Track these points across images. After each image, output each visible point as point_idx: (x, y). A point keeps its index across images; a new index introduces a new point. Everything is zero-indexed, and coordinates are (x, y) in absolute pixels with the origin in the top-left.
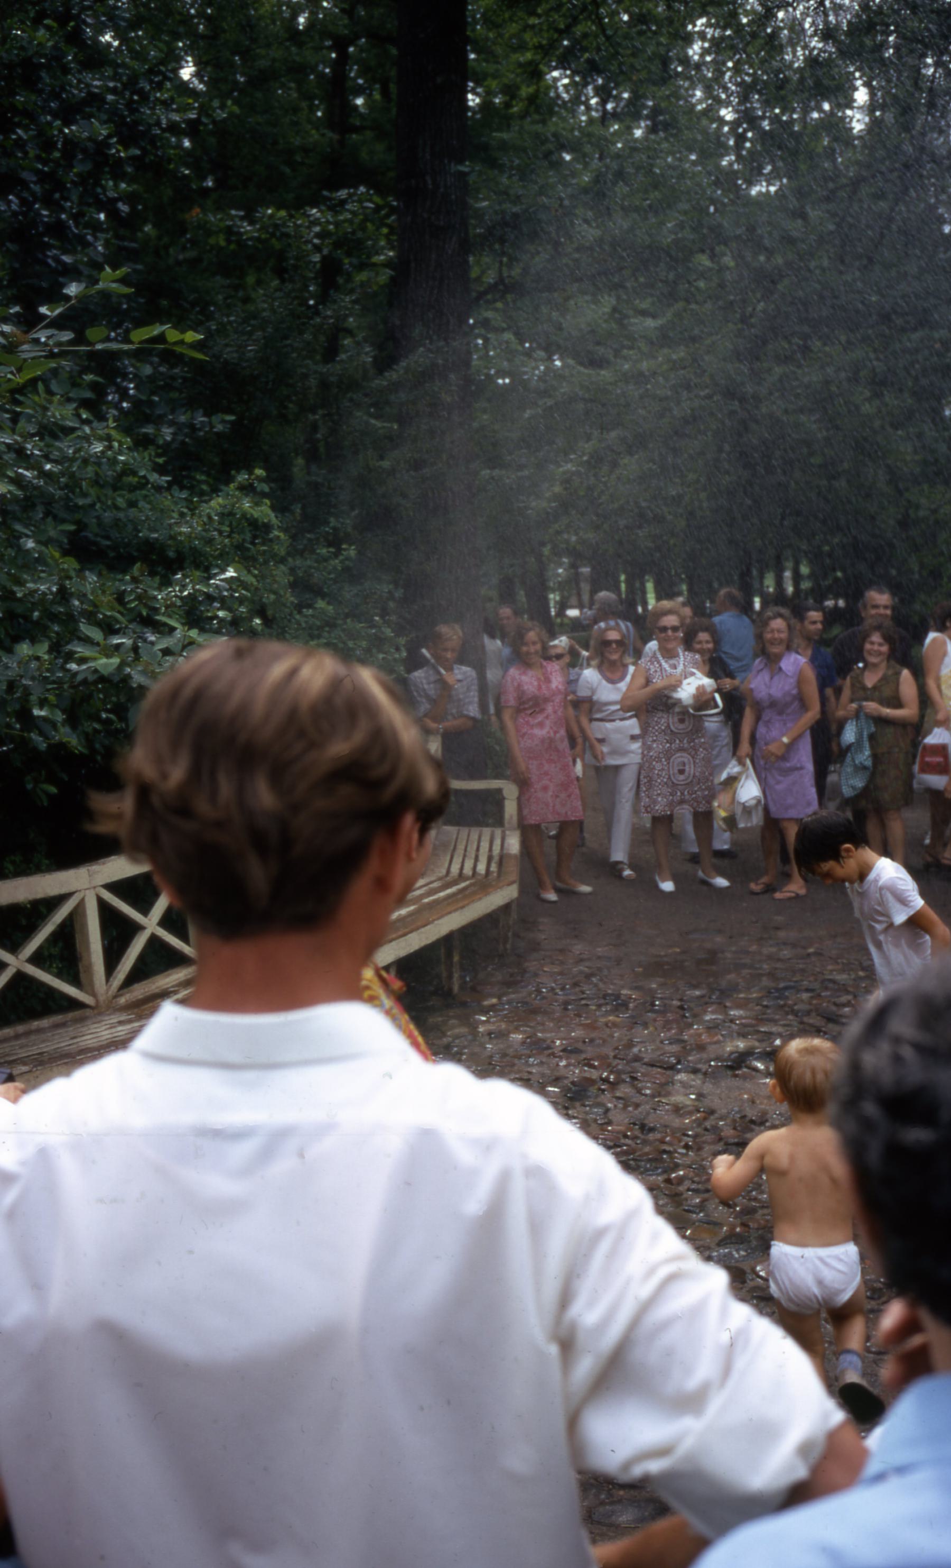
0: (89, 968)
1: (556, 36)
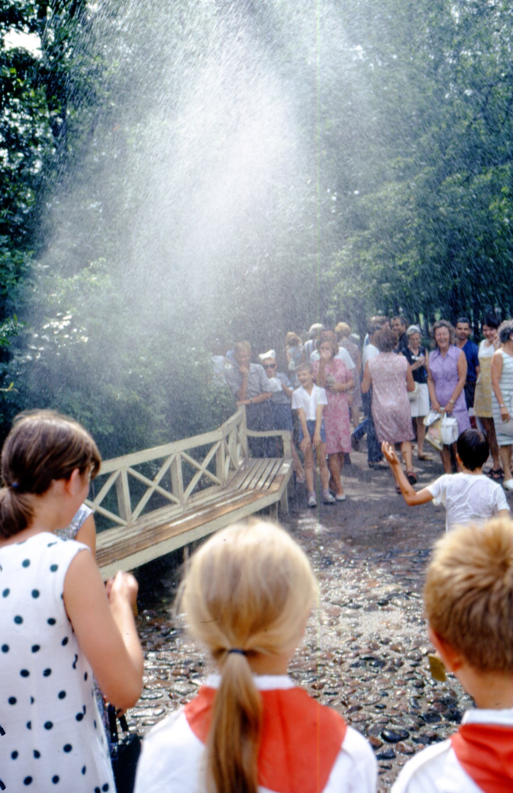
0: (123, 506)
1: (417, 45)
